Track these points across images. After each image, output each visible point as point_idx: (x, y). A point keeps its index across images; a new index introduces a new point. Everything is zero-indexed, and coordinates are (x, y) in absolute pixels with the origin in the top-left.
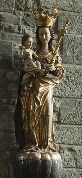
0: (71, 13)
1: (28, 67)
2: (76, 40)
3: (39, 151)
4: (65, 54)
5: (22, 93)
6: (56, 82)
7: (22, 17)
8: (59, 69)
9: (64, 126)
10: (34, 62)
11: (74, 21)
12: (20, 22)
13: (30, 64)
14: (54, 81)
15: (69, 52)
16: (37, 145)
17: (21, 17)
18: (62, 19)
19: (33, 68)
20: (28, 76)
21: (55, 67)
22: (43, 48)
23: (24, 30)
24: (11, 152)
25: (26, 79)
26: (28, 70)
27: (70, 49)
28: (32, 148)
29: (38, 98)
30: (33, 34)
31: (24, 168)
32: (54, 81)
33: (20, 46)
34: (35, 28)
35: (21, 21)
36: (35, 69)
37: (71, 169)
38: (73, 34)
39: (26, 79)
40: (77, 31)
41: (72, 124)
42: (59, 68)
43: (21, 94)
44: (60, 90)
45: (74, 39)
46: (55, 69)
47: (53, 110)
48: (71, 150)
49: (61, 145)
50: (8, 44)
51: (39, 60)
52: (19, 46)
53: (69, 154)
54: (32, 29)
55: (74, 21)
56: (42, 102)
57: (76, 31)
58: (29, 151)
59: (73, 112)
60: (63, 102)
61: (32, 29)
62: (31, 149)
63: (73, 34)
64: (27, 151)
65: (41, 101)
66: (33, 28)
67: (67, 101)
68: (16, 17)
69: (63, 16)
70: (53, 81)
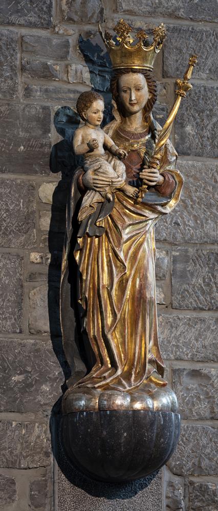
0: (195, 24)
1: (96, 177)
2: (209, 94)
3: (125, 388)
4: (181, 133)
5: (80, 240)
6: (164, 211)
7: (73, 40)
8: (171, 179)
9: (180, 316)
10: (110, 163)
11: (204, 45)
12: (68, 52)
13: (101, 170)
14: (159, 208)
15: (193, 126)
16: (119, 372)
17: (70, 41)
18: (173, 41)
19: (108, 180)
20: (95, 200)
21: (162, 174)
22: (129, 123)
23: (79, 74)
24: (52, 386)
25: (90, 206)
26: (94, 183)
27: (195, 119)
28: (108, 381)
29: (122, 256)
30: (101, 82)
31: (89, 430)
32: (159, 208)
33: (69, 114)
34: (106, 67)
35: (71, 49)
36: (112, 182)
37: (199, 425)
38: (202, 79)
39: (90, 206)
40: (210, 70)
41: (202, 309)
42: (170, 176)
43: (79, 245)
44: (171, 224)
45: (202, 92)
46: (161, 178)
47: (156, 277)
48: (195, 374)
49: (175, 362)
50: (41, 110)
51: (120, 157)
52: (67, 116)
53: (194, 387)
54: (99, 71)
55: (204, 45)
56: (129, 263)
57: (207, 72)
58: (99, 387)
59: (204, 279)
60: (178, 254)
61: (99, 71)
62: (104, 383)
63: (202, 79)
64: (94, 388)
65: (128, 261)
66: (100, 68)
67: (186, 251)
68: (59, 41)
69: (176, 34)
70: (156, 209)
